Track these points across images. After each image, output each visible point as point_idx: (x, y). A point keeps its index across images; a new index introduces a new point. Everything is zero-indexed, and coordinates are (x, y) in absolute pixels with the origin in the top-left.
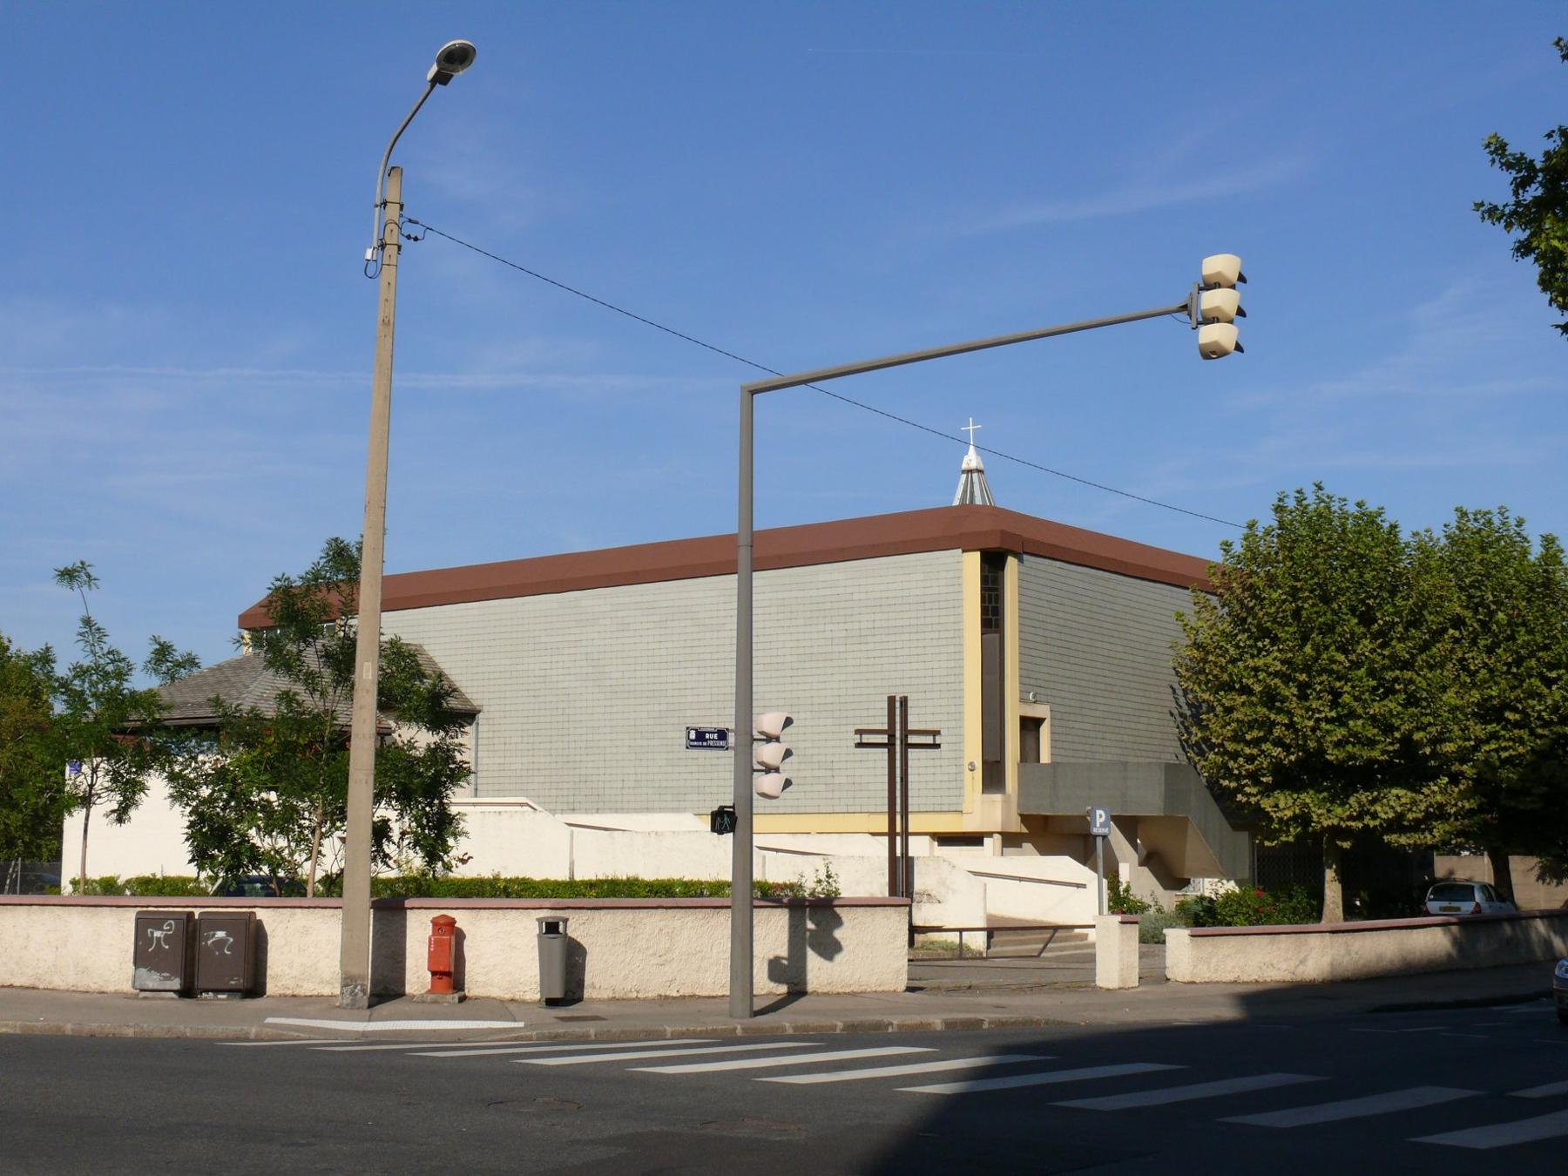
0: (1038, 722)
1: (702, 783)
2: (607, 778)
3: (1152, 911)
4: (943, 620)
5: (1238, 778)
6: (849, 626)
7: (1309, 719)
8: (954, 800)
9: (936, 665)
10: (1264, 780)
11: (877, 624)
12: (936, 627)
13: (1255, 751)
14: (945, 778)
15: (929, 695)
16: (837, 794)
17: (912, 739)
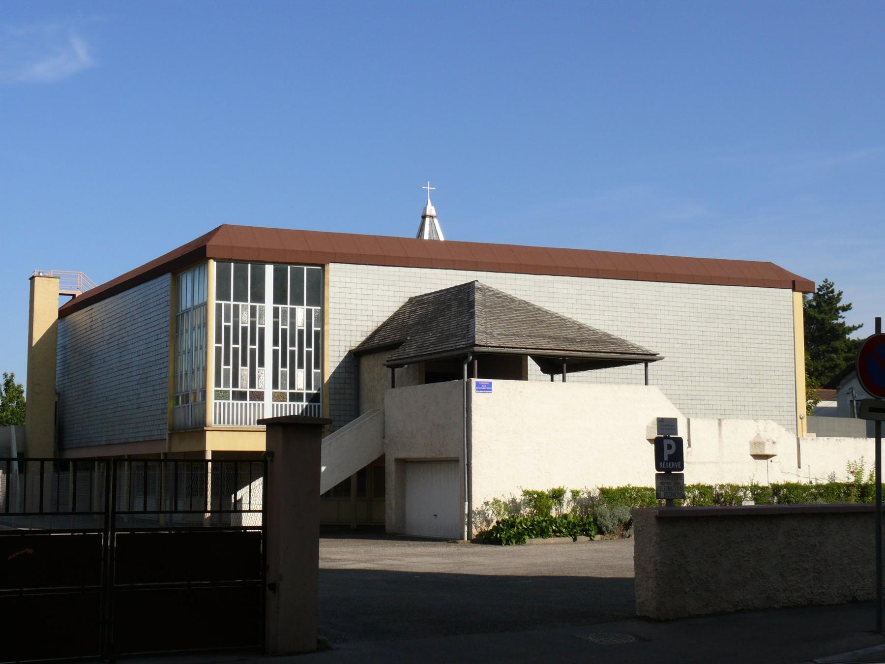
6: (732, 326)
9: (780, 355)
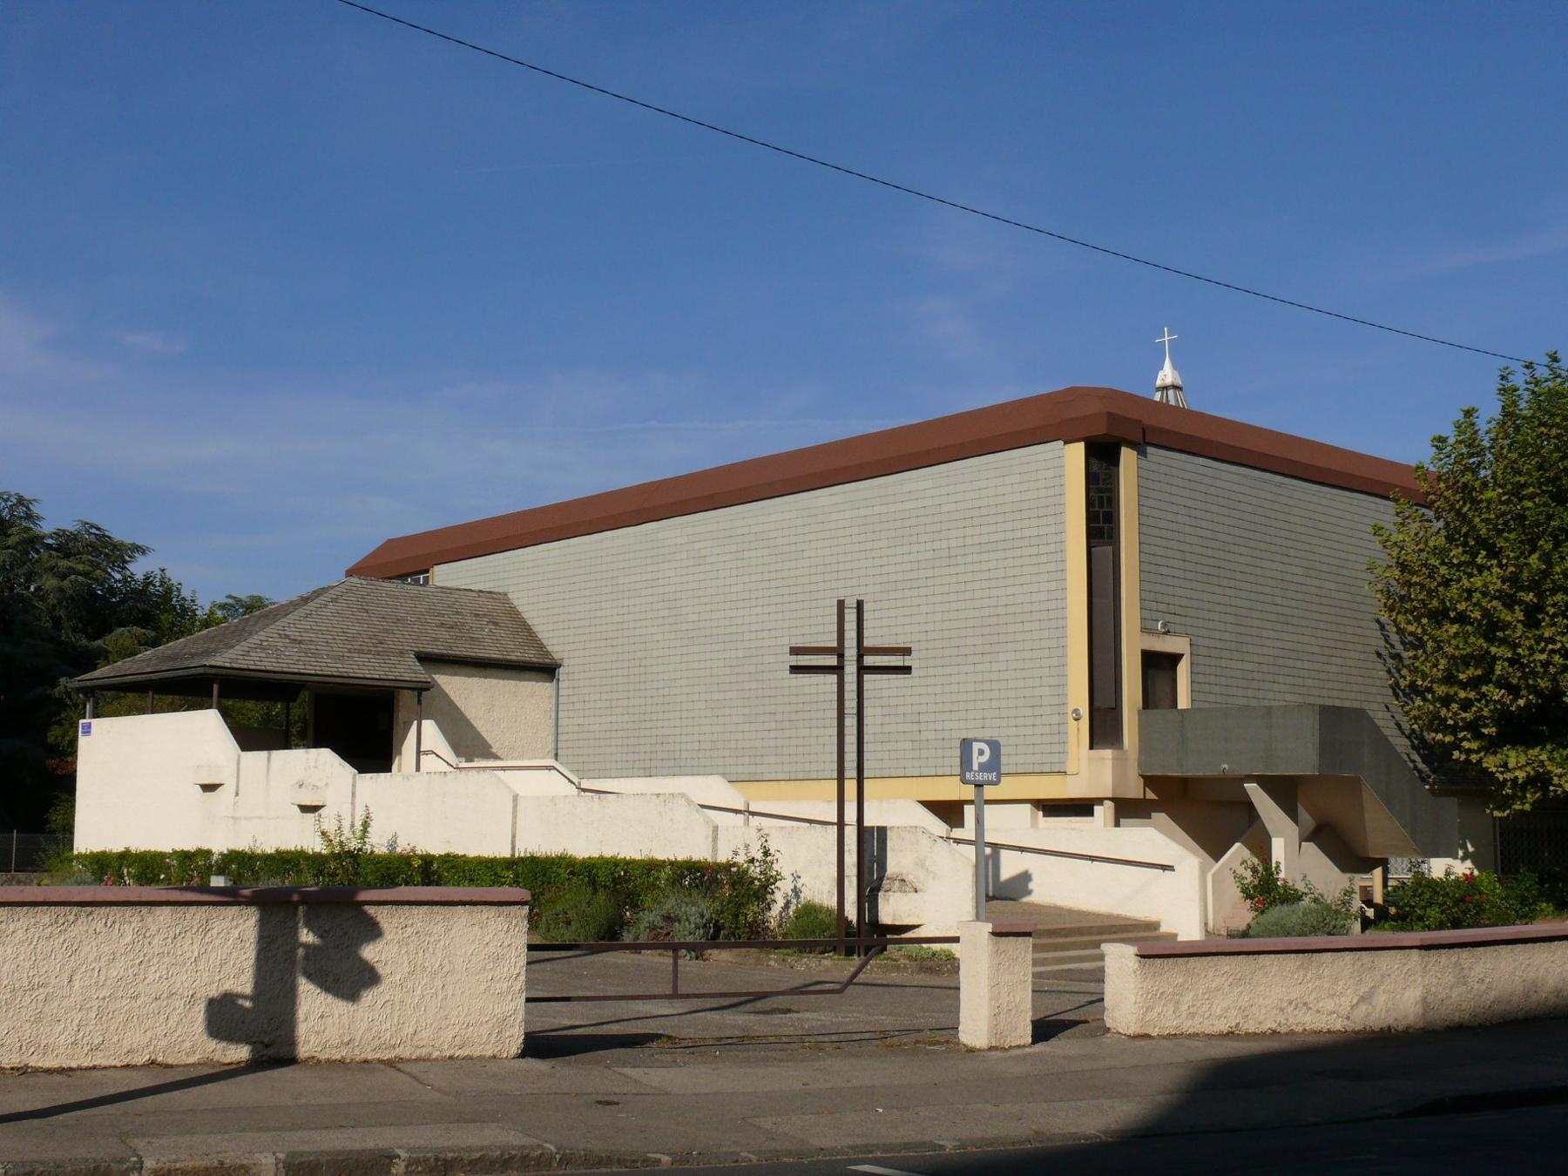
0: (1175, 659)
1: (780, 742)
2: (684, 738)
3: (1306, 901)
4: (1043, 531)
5: (1454, 730)
6: (937, 545)
7: (1542, 651)
8: (1055, 758)
9: (1035, 588)
10: (1486, 731)
11: (969, 541)
12: (1034, 541)
13: (1472, 695)
14: (1046, 730)
15: (1027, 626)
16: (924, 753)
17: (869, 660)
